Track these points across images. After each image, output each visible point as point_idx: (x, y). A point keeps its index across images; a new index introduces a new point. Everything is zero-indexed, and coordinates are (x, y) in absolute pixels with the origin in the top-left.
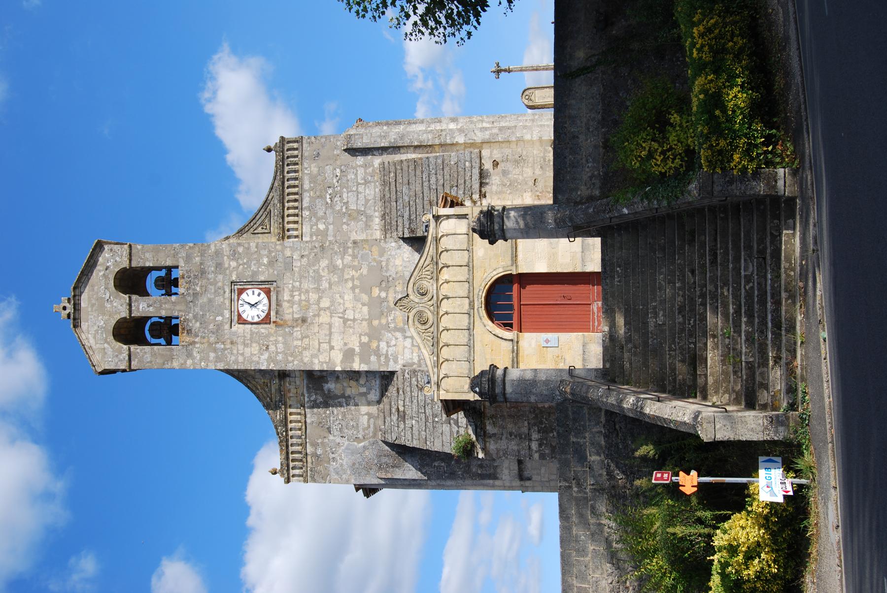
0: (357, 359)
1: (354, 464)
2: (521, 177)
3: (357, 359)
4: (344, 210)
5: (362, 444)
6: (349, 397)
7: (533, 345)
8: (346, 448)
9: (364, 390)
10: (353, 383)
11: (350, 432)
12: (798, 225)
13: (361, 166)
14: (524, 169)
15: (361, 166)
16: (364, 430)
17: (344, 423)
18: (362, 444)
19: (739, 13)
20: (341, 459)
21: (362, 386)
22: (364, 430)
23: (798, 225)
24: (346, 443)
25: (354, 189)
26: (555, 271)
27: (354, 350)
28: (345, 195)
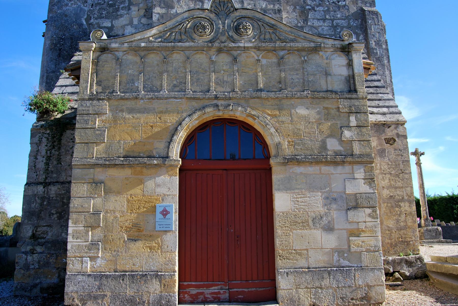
0: (163, 11)
1: (66, 16)
2: (378, 171)
3: (163, 11)
4: (307, 7)
5: (85, 23)
6: (129, 9)
7: (158, 190)
8: (81, 9)
9: (135, 22)
10: (142, 12)
11: (96, 12)
12: (264, 289)
13: (349, 24)
14: (388, 176)
15: (349, 24)
16: (98, 24)
17: (104, 6)
18: (85, 23)
19: (43, 100)
20: (72, 4)
21: (140, 21)
22: (98, 24)
23: (264, 289)
24: (86, 9)
25: (327, 17)
26: (258, 130)
27: (173, 8)
28: (321, 8)
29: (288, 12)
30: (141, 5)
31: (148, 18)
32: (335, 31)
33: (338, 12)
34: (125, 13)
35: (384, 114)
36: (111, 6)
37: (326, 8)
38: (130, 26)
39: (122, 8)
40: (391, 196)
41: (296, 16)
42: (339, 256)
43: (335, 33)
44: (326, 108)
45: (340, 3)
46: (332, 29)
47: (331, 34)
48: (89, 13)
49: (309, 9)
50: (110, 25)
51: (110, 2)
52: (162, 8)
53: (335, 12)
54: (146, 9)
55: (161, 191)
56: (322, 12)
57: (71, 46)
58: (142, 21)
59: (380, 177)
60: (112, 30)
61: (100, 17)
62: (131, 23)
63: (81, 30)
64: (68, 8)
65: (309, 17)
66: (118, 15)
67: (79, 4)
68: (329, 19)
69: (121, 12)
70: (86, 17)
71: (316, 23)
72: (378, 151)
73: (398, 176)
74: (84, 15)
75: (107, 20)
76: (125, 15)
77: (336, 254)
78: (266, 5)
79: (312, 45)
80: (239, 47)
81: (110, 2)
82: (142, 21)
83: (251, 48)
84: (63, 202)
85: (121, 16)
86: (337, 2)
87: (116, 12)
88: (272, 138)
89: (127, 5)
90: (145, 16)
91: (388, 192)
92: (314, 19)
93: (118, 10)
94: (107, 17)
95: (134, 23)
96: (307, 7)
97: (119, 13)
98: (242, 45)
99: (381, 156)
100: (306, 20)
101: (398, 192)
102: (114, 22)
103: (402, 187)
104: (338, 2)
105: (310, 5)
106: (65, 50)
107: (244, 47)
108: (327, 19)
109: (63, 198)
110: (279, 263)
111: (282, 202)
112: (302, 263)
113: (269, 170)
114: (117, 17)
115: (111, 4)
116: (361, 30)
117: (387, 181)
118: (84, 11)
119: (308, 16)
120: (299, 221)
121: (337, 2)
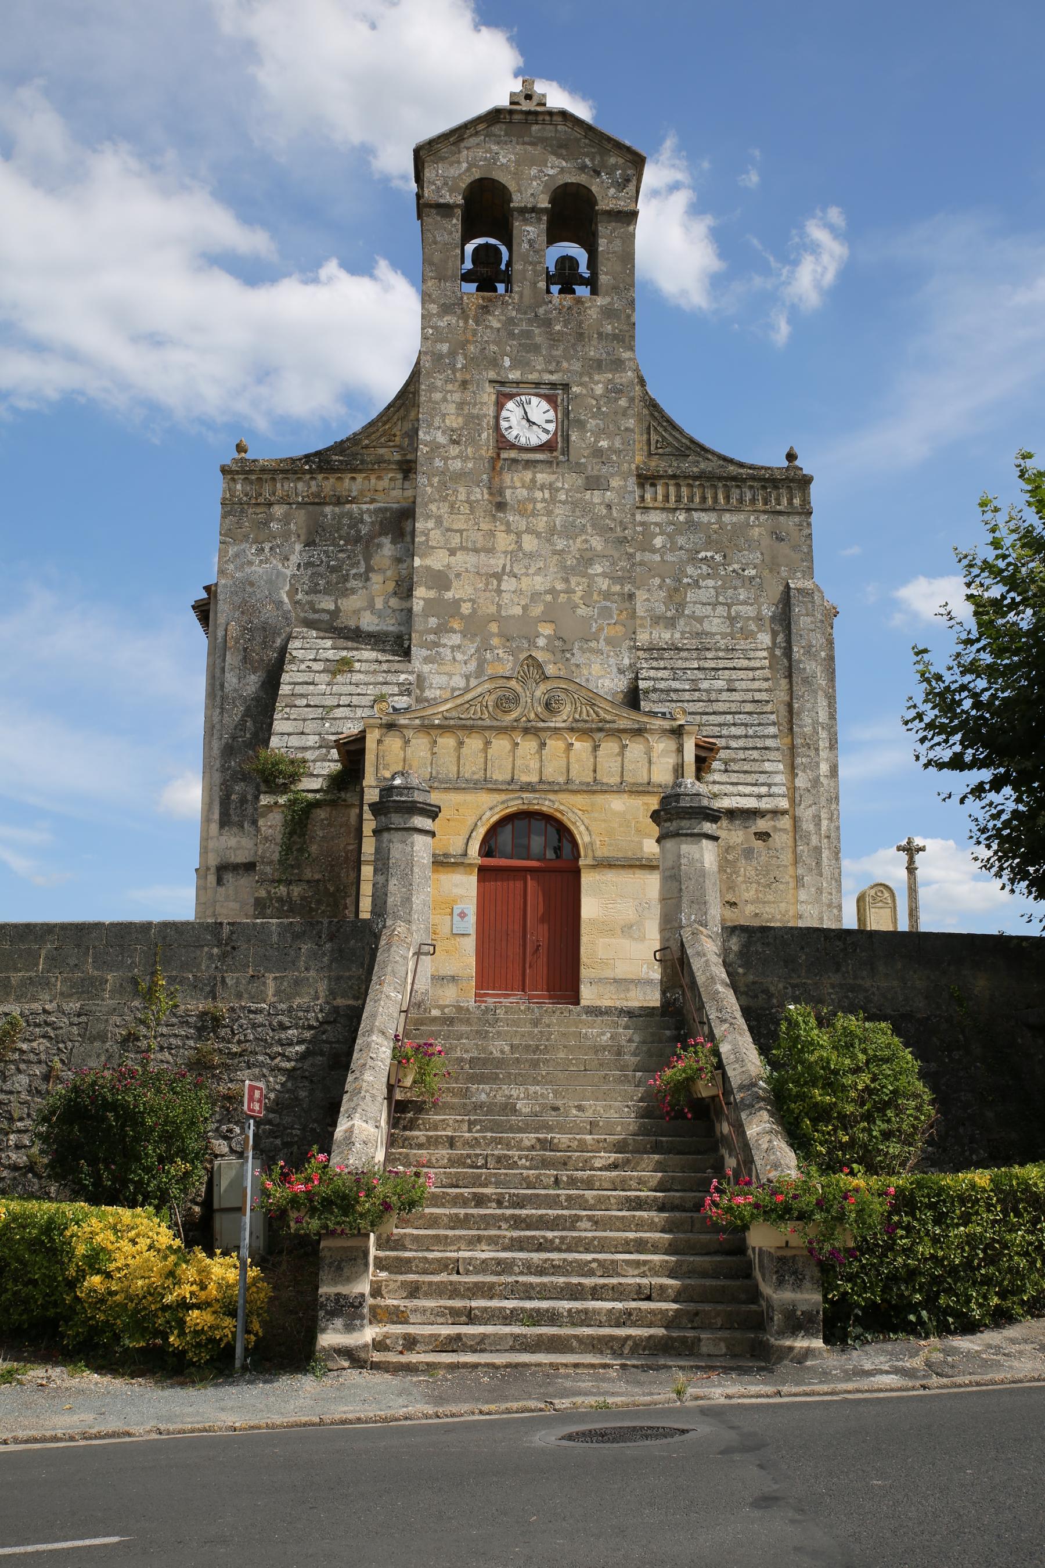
0: (432, 594)
1: (252, 584)
3: (432, 594)
4: (685, 580)
5: (286, 600)
6: (367, 579)
8: (279, 574)
9: (379, 604)
10: (391, 586)
14: (754, 886)
28: (710, 583)
29: (649, 590)
30: (389, 573)
31: (401, 598)
32: (732, 625)
33: (741, 591)
34: (360, 585)
35: (760, 796)
36: (333, 570)
37: (720, 583)
38: (369, 612)
39: (354, 575)
40: (757, 915)
41: (665, 597)
42: (648, 968)
43: (732, 630)
44: (646, 804)
45: (746, 572)
46: (728, 623)
47: (725, 633)
48: (293, 582)
49: (689, 584)
50: (332, 607)
51: (332, 563)
52: (429, 588)
53: (735, 589)
54: (397, 581)
55: (458, 891)
56: (712, 590)
57: (264, 642)
58: (390, 604)
59: (744, 886)
60: (337, 617)
61: (315, 591)
62: (371, 606)
63: (280, 613)
64: (253, 568)
65: (688, 600)
66: (347, 590)
67: (275, 562)
68: (723, 604)
69: (352, 583)
70: (287, 588)
71: (700, 611)
72: (744, 850)
73: (769, 886)
74: (285, 585)
75: (327, 598)
76: (360, 591)
77: (645, 966)
78: (609, 585)
79: (636, 726)
80: (548, 728)
81: (332, 563)
82: (390, 604)
83: (563, 728)
84: (310, 907)
85: (353, 591)
86: (740, 571)
87: (344, 583)
88: (583, 838)
89: (362, 570)
90: (395, 593)
91: (752, 908)
92: (695, 603)
93: (346, 579)
94: (326, 592)
95: (377, 607)
96: (685, 580)
97: (349, 585)
98: (552, 725)
99: (746, 858)
100: (681, 606)
101: (767, 909)
102: (339, 601)
103: (773, 902)
104: (744, 570)
105: (691, 577)
106: (254, 651)
107: (555, 728)
108: (721, 604)
109: (311, 902)
110: (584, 973)
111: (590, 908)
112: (609, 974)
113: (577, 873)
114: (346, 593)
115: (333, 566)
116: (781, 625)
117: (752, 893)
118: (285, 576)
119: (686, 597)
120: (606, 929)
121: (740, 571)
